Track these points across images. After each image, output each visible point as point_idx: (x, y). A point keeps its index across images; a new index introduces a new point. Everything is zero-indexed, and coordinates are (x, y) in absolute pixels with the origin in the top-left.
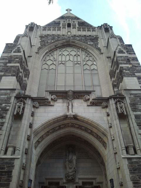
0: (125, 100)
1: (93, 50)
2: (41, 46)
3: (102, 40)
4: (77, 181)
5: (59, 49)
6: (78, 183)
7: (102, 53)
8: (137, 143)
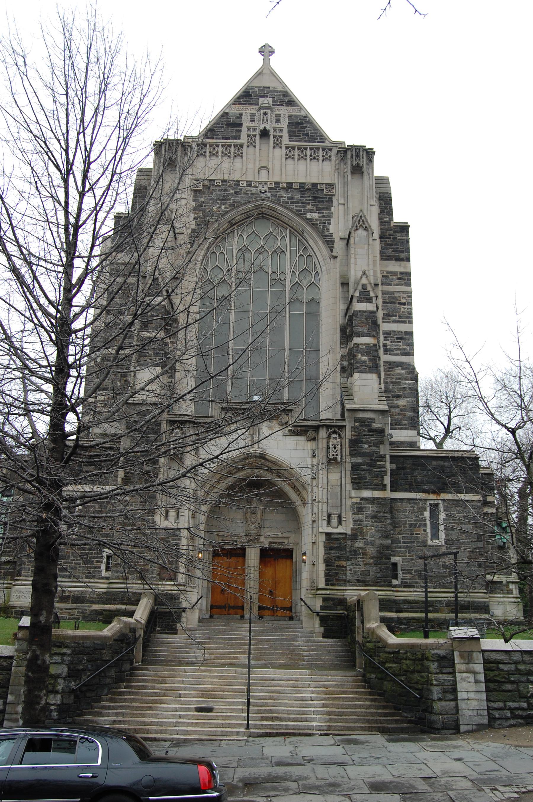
0: (344, 431)
1: (316, 243)
2: (197, 225)
3: (341, 207)
4: (262, 539)
5: (238, 226)
6: (262, 543)
7: (335, 257)
8: (344, 511)
